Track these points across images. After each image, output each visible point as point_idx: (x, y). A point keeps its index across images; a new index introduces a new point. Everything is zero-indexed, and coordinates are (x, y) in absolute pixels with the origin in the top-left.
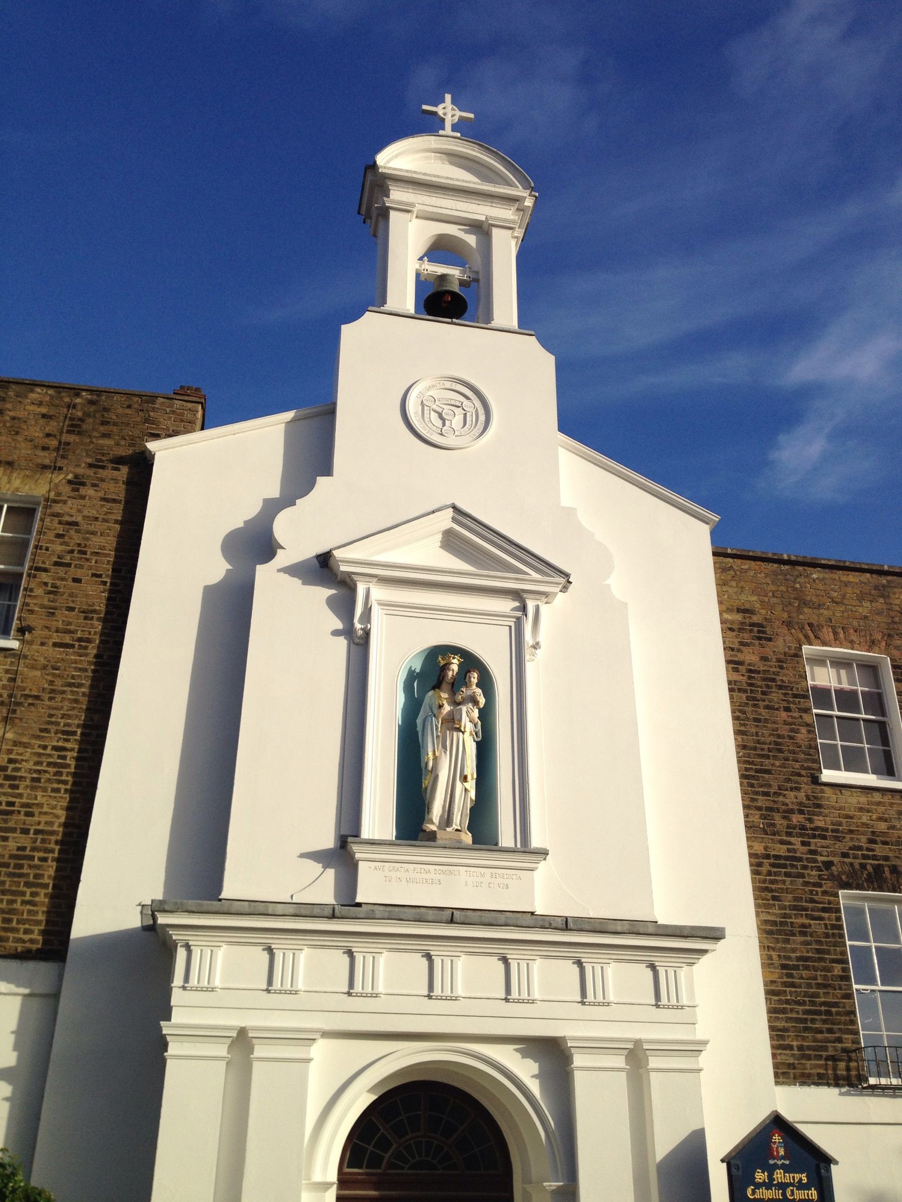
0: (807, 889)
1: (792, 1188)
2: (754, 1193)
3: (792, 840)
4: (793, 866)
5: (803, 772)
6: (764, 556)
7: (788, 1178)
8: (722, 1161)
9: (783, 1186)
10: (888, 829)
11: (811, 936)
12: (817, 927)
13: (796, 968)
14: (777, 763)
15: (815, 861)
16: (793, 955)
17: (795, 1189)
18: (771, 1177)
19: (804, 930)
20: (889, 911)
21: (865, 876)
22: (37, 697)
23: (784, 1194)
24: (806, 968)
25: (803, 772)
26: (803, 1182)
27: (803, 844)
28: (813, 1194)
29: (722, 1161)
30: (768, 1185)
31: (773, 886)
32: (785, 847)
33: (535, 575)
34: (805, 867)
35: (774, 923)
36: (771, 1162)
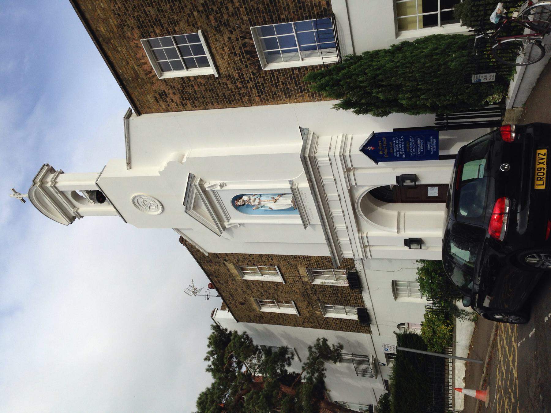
0: (267, 82)
2: (386, 155)
3: (249, 87)
4: (260, 87)
6: (98, 37)
7: (380, 146)
9: (383, 147)
10: (226, 46)
11: (286, 81)
12: (281, 79)
13: (300, 87)
14: (218, 91)
15: (254, 78)
16: (296, 88)
18: (381, 150)
19: (284, 84)
20: (342, 407)
21: (252, 59)
22: (288, 262)
23: (385, 147)
24: (299, 84)
27: (248, 82)
29: (378, 163)
32: (253, 89)
33: (195, 190)
34: (258, 83)
35: (285, 95)
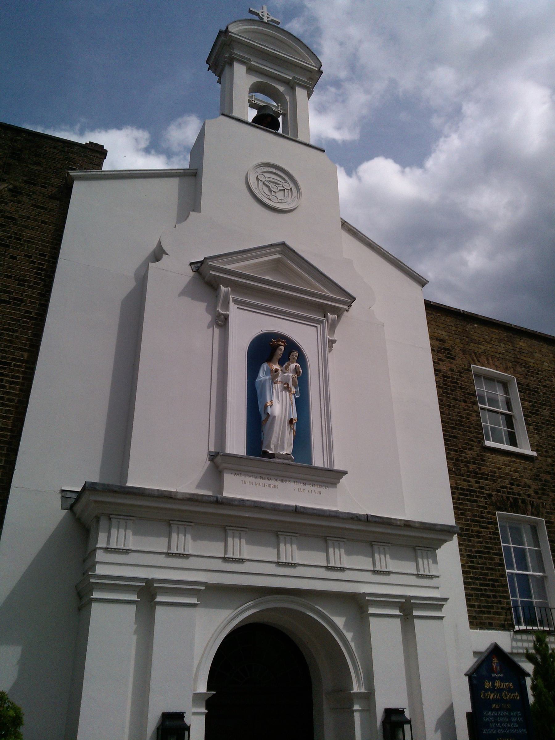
1: (505, 692)
5: (475, 440)
8: (466, 675)
9: (500, 691)
17: (507, 692)
25: (475, 440)
26: (511, 688)
28: (517, 696)
30: (492, 690)
31: (461, 507)
32: (466, 483)
36: (493, 675)
